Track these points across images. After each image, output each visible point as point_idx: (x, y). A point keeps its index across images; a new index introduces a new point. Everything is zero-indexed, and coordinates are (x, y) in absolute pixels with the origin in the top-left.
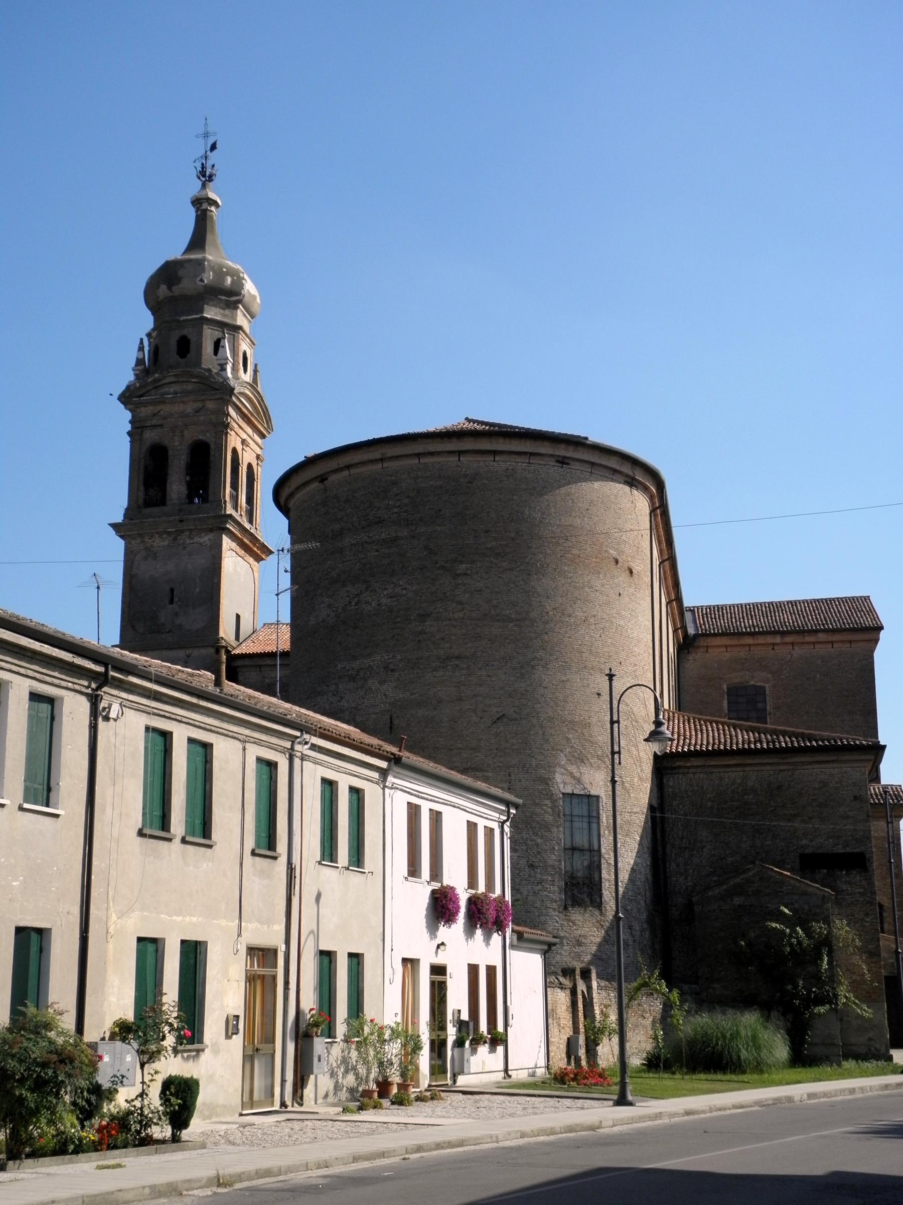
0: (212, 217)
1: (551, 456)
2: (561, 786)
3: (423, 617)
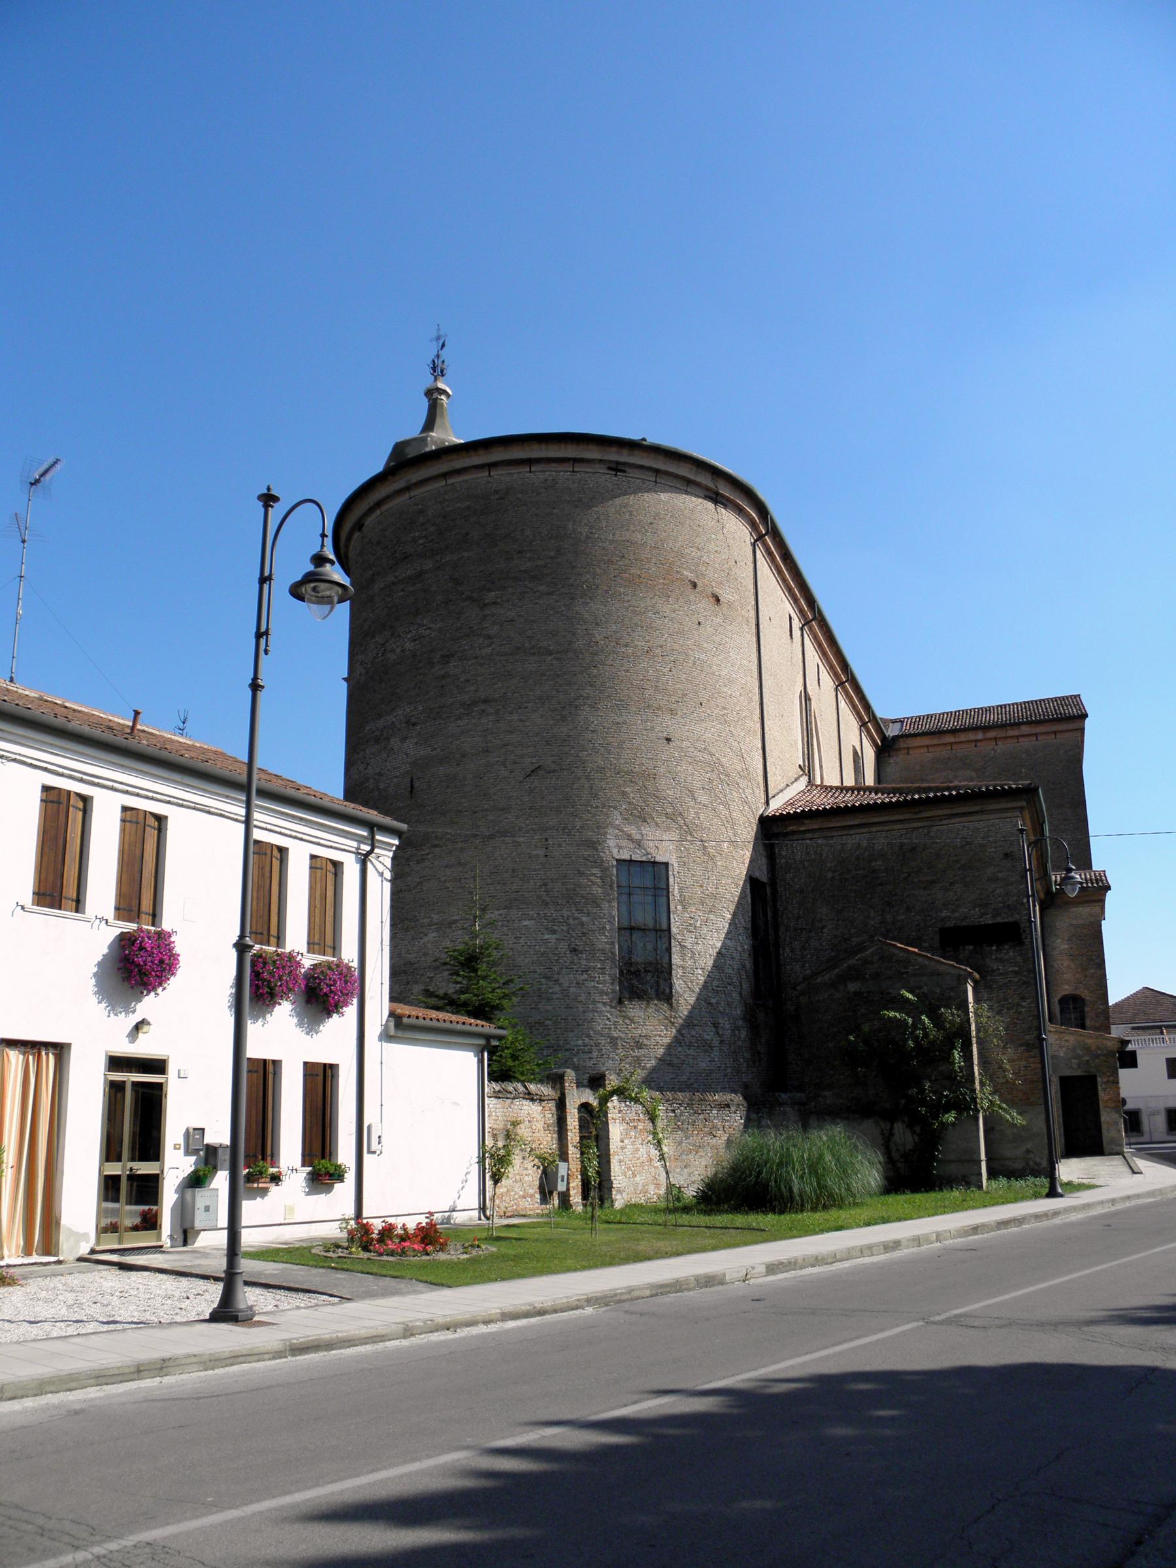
0: (442, 405)
1: (601, 461)
2: (615, 851)
3: (446, 658)
